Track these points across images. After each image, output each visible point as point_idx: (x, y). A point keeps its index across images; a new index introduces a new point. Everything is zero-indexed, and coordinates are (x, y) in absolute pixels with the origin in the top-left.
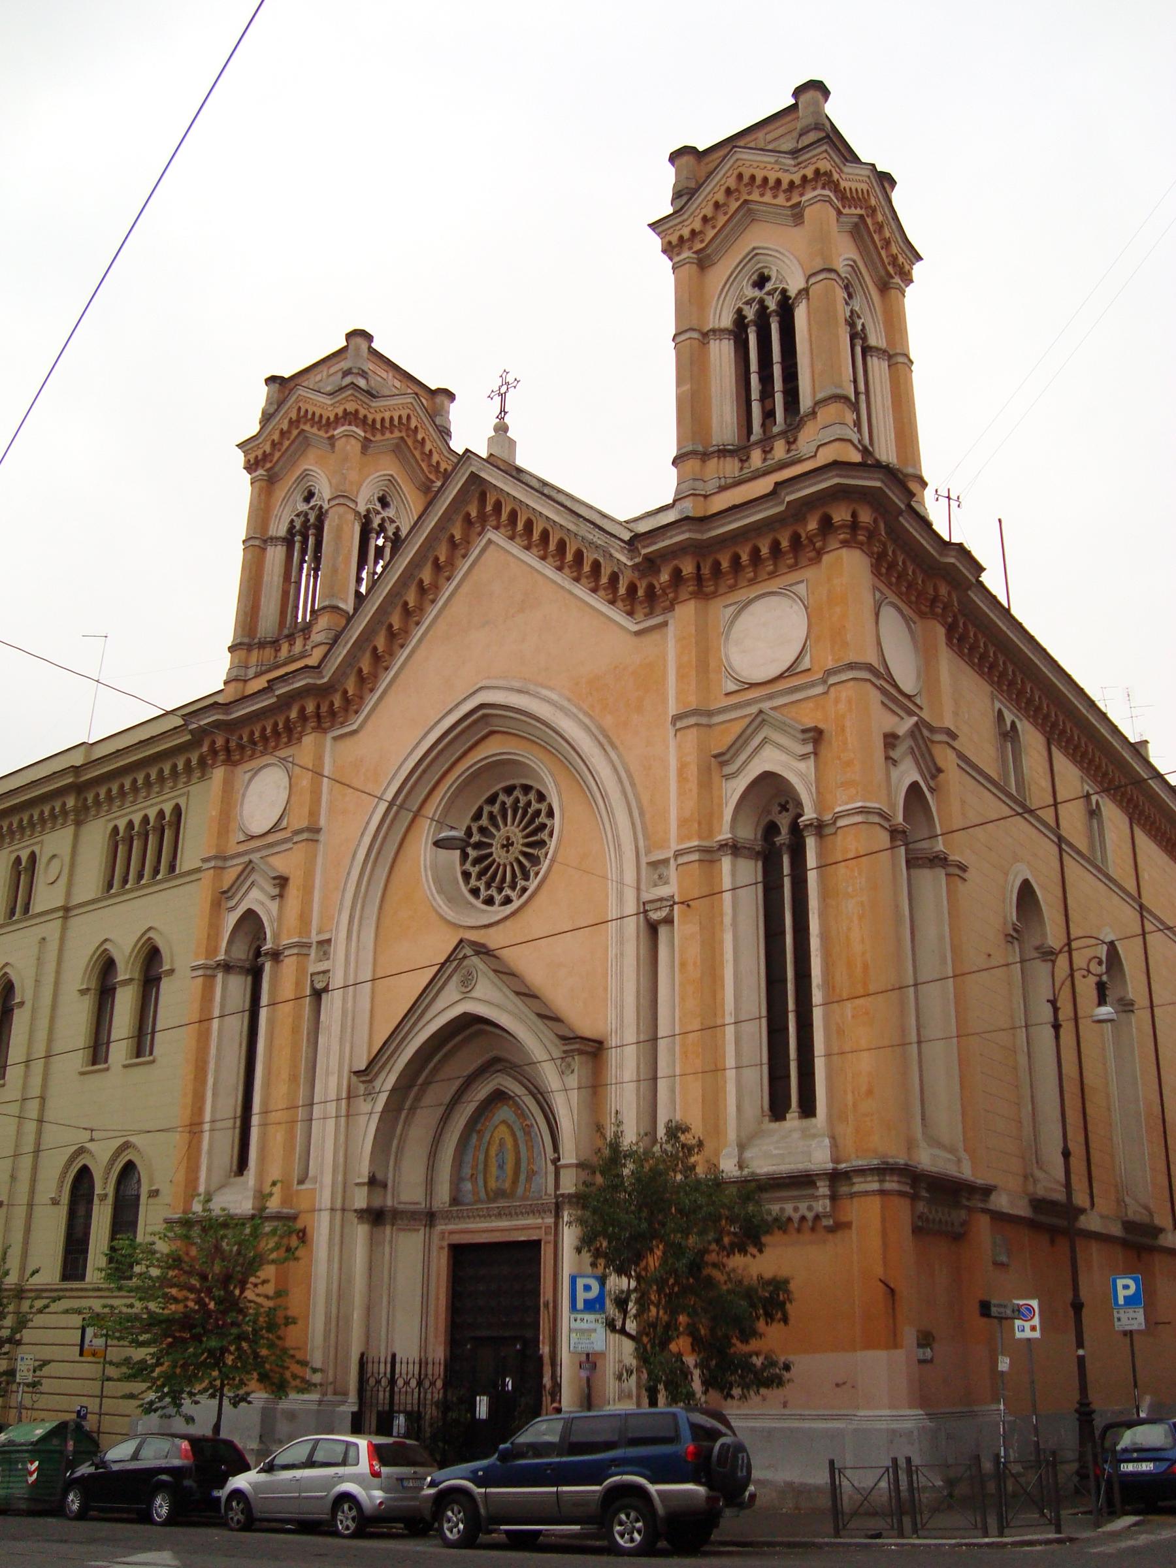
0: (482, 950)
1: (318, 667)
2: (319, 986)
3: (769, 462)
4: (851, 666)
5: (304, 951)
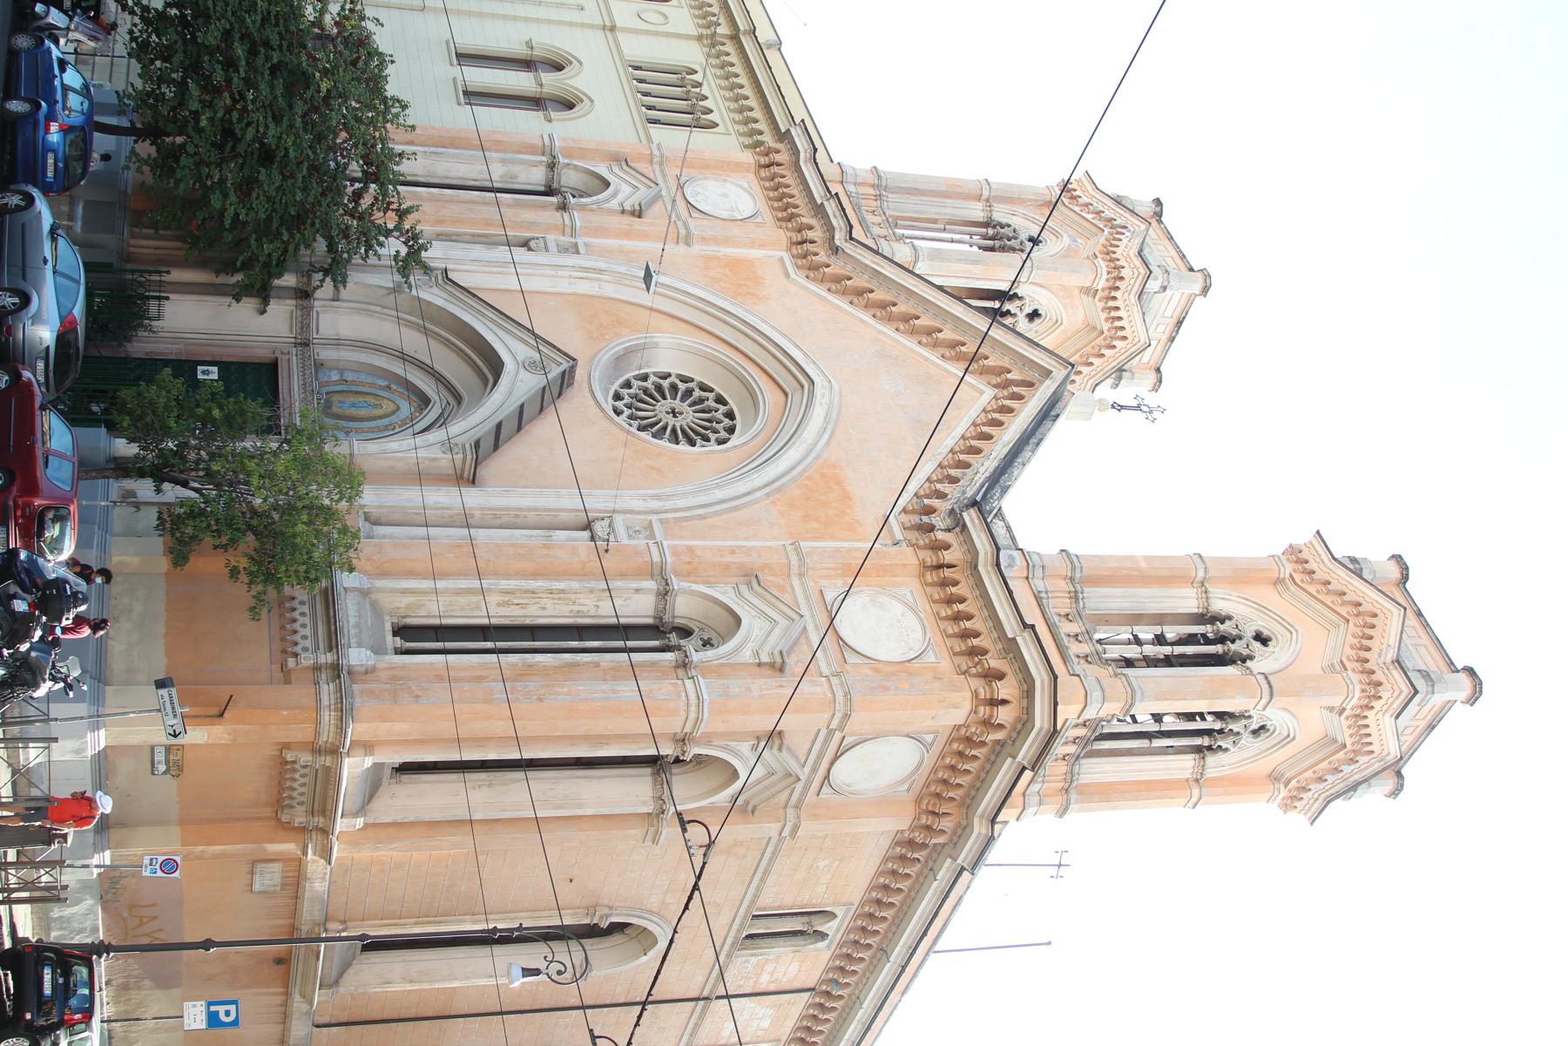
0: (566, 379)
1: (851, 238)
2: (532, 244)
3: (1066, 639)
4: (847, 694)
5: (568, 230)
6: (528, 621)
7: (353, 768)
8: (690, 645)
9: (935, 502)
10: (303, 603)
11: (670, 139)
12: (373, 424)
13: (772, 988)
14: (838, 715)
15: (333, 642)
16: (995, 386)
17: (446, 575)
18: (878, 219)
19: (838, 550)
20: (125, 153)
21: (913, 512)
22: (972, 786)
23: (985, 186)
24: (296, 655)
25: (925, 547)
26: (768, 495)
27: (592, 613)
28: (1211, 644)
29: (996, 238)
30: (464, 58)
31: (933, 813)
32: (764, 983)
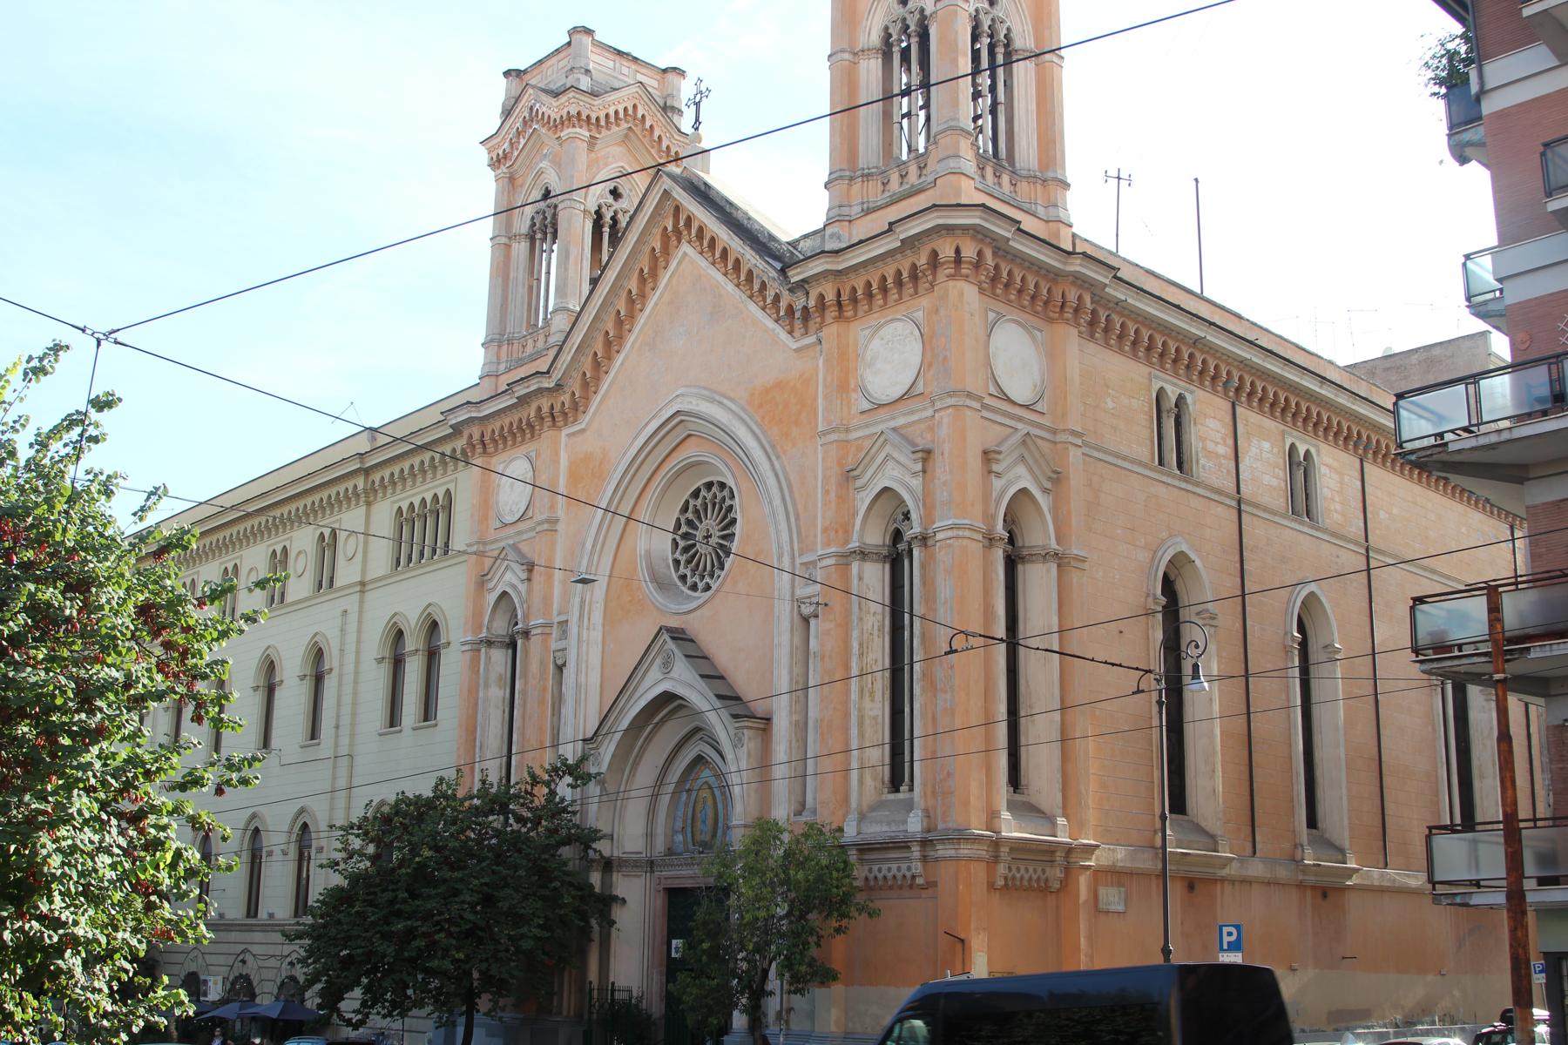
0: (679, 636)
2: (560, 662)
3: (906, 187)
4: (951, 394)
5: (547, 630)
7: (1012, 829)
8: (908, 535)
9: (783, 304)
10: (870, 870)
11: (461, 537)
12: (720, 806)
13: (1230, 442)
14: (969, 402)
15: (902, 845)
16: (679, 242)
17: (847, 741)
18: (530, 342)
19: (825, 397)
20: (488, 1020)
21: (792, 325)
22: (1037, 273)
23: (497, 240)
24: (914, 877)
25: (823, 316)
26: (778, 457)
27: (880, 617)
29: (545, 229)
30: (394, 719)
32: (1225, 450)
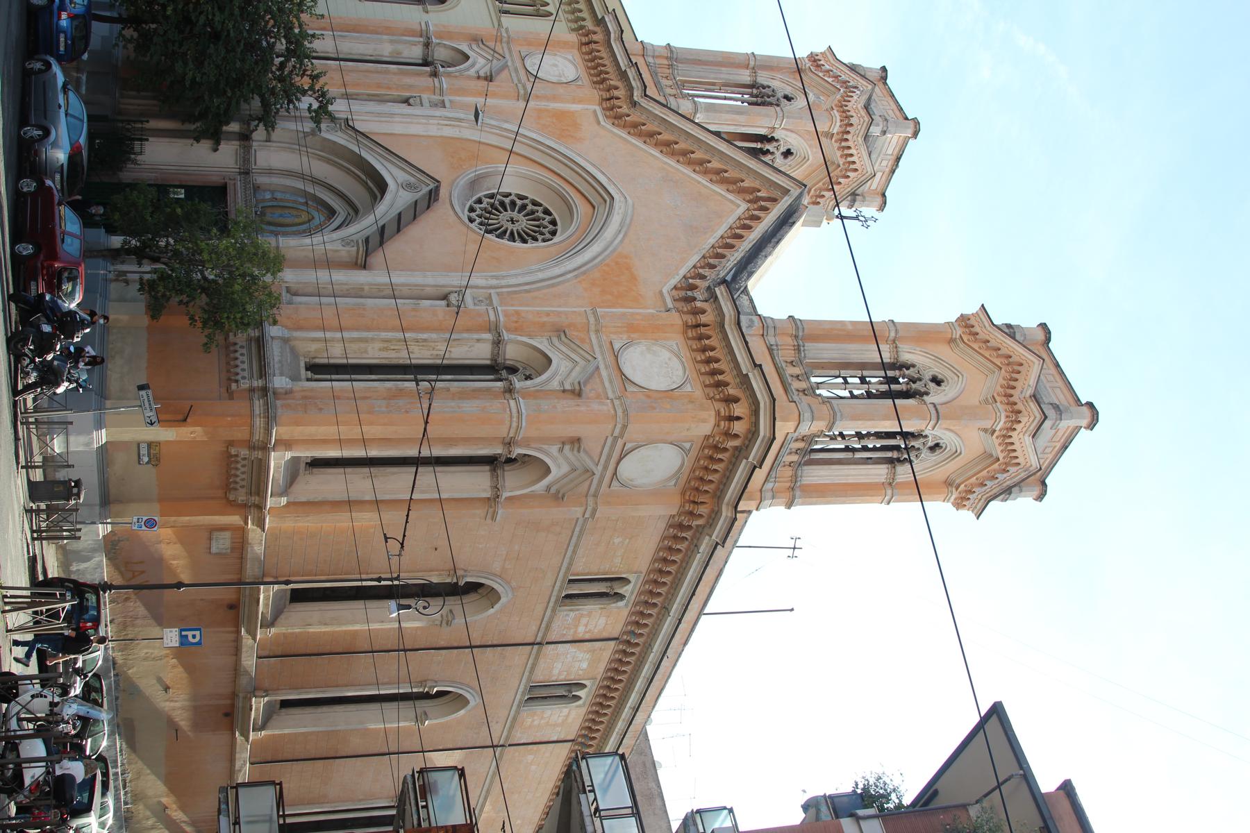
2: (411, 101)
4: (625, 412)
5: (437, 91)
6: (401, 362)
7: (277, 462)
9: (698, 282)
12: (294, 229)
13: (587, 637)
14: (619, 426)
15: (263, 372)
18: (670, 83)
19: (624, 314)
21: (682, 289)
22: (720, 482)
24: (237, 381)
26: (576, 277)
28: (898, 383)
29: (761, 96)
31: (694, 502)
32: (581, 632)
